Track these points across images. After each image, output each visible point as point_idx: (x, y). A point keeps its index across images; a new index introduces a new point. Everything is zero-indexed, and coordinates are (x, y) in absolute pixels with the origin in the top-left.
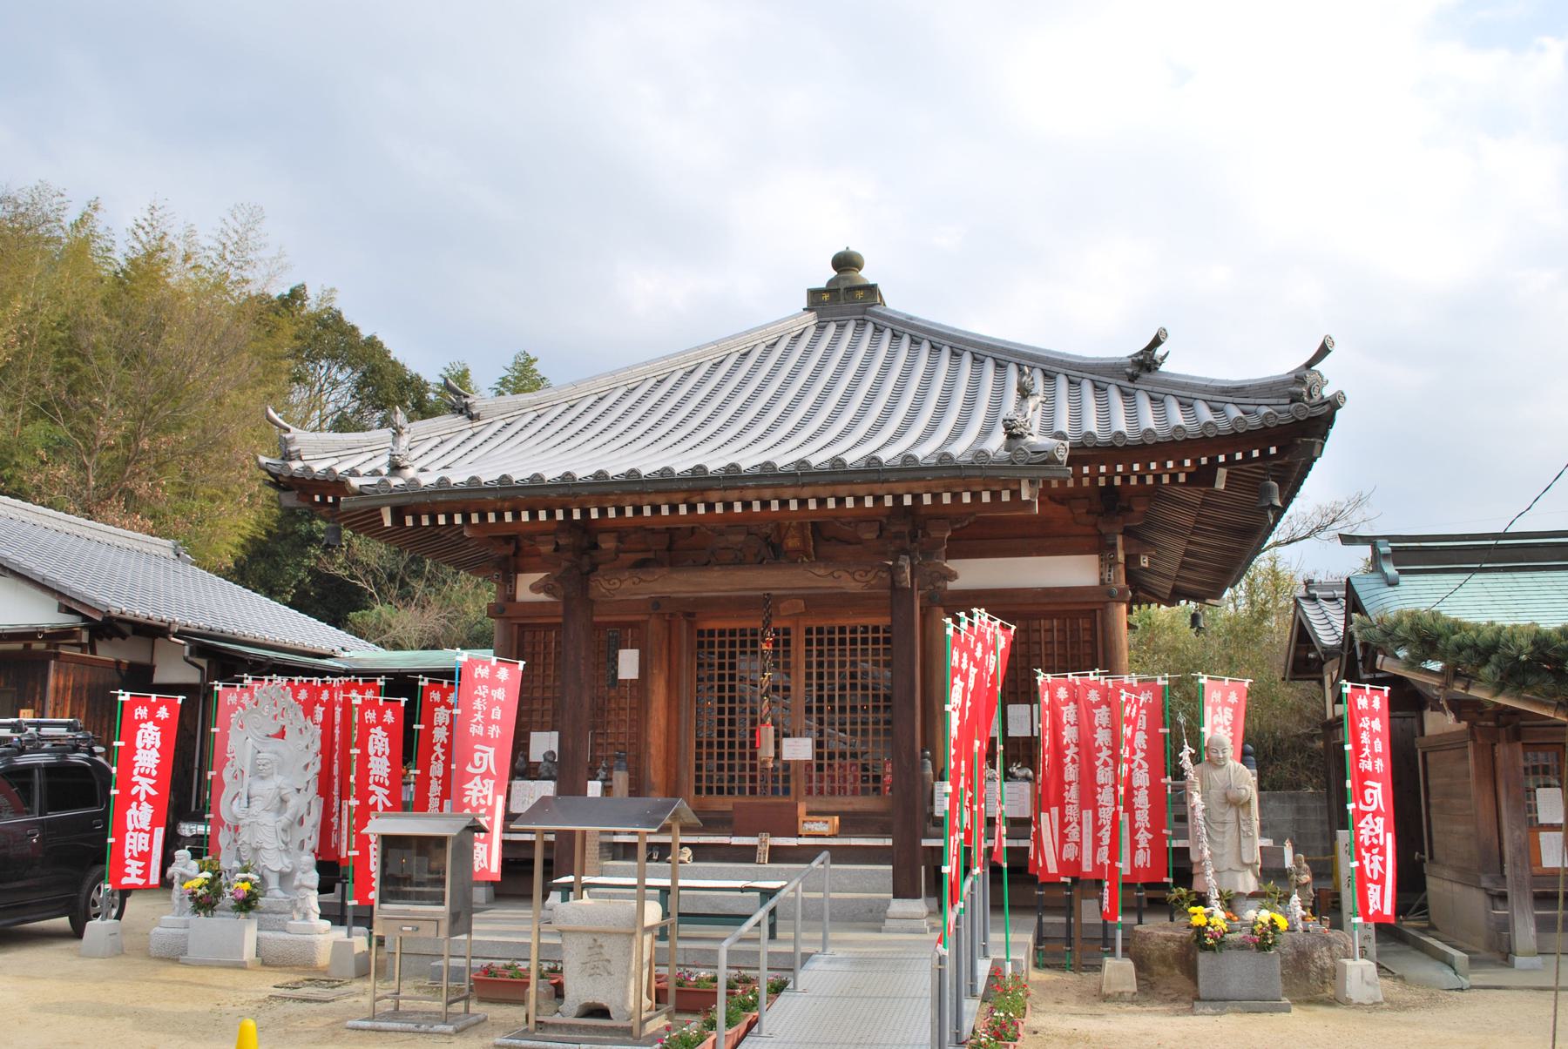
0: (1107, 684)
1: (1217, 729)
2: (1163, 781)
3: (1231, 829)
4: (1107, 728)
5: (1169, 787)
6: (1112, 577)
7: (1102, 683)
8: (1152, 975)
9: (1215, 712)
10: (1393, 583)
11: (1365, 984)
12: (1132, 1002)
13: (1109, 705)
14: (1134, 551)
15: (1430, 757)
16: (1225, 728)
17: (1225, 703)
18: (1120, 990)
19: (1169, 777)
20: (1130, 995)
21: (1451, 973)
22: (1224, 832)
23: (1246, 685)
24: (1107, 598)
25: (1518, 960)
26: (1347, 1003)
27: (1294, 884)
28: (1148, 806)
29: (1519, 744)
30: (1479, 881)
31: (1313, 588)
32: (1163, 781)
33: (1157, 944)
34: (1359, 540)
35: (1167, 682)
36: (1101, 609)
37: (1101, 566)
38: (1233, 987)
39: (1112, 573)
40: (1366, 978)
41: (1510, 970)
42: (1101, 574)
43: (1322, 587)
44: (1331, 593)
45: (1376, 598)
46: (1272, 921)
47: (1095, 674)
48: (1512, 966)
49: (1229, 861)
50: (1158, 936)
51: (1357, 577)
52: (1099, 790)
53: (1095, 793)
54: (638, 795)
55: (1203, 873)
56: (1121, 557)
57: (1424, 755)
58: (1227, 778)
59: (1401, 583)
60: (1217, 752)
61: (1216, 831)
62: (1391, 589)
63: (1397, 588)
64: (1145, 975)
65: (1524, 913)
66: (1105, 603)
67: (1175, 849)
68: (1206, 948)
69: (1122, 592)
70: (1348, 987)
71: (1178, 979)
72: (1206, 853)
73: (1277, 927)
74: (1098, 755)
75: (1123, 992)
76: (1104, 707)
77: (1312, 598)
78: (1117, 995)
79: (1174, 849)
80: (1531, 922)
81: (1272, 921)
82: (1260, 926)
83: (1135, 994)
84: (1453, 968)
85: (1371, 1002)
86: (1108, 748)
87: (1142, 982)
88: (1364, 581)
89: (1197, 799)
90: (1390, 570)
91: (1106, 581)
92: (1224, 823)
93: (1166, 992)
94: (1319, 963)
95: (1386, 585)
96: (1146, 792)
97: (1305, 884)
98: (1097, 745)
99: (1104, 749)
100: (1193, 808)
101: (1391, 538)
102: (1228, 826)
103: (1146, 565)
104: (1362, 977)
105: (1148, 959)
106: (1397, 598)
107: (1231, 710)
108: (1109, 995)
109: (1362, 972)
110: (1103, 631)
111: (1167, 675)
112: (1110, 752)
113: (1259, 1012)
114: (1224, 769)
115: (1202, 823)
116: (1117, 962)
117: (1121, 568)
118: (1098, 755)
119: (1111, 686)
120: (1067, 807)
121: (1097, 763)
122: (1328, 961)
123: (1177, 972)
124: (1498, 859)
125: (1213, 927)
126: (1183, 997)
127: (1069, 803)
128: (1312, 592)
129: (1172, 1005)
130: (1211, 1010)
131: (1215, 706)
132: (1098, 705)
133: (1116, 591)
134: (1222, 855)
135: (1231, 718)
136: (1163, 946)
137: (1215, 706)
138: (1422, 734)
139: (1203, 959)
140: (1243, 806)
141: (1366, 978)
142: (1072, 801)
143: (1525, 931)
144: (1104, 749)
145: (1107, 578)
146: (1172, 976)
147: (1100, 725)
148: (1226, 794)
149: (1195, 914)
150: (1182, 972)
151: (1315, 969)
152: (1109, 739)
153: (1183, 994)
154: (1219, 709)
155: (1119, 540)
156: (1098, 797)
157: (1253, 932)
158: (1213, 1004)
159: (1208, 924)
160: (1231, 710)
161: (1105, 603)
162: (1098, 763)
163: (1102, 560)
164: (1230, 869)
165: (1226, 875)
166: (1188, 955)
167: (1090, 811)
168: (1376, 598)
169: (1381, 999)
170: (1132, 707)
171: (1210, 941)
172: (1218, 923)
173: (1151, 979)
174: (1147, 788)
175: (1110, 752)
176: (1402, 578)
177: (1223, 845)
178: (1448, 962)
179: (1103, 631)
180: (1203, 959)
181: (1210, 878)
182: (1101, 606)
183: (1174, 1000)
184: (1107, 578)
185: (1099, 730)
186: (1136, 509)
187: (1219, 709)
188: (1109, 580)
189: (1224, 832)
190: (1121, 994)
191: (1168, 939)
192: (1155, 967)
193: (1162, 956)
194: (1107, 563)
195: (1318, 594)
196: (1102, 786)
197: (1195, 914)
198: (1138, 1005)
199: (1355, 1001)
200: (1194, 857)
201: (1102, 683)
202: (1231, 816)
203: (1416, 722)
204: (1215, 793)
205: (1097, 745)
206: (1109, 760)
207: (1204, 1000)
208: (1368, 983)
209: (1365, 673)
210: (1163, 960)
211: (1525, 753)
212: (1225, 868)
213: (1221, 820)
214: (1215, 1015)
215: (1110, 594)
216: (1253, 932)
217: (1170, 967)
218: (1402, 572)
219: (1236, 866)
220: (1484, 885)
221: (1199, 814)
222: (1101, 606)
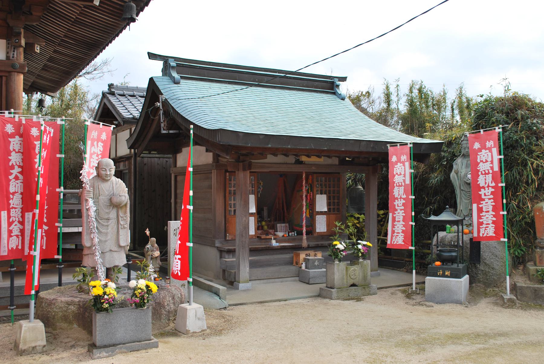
0: (20, 120)
1: (93, 156)
2: (58, 190)
3: (112, 223)
4: (19, 152)
5: (62, 194)
6: (15, 56)
7: (17, 119)
8: (55, 329)
9: (92, 145)
10: (176, 83)
11: (197, 320)
12: (43, 352)
13: (21, 136)
14: (31, 41)
15: (179, 178)
16: (98, 156)
17: (99, 140)
18: (33, 345)
19: (62, 188)
20: (41, 347)
21: (217, 298)
22: (108, 226)
23: (112, 129)
24: (11, 69)
25: (241, 286)
26: (186, 333)
27: (149, 258)
28: (21, 206)
29: (248, 172)
30: (214, 244)
31: (113, 88)
32: (58, 190)
33: (60, 308)
34: (158, 57)
35: (63, 123)
36: (6, 76)
37: (8, 48)
38: (120, 334)
39: (15, 53)
40: (198, 316)
41: (237, 291)
42: (8, 53)
43: (118, 88)
44: (122, 92)
45: (169, 89)
46: (147, 286)
47: (10, 113)
48: (238, 289)
49: (111, 244)
50: (62, 301)
51: (157, 77)
52: (11, 196)
53: (9, 199)
54: (469, 156)
55: (93, 254)
56: (23, 42)
57: (176, 177)
58: (111, 189)
59: (181, 83)
60: (106, 170)
61: (103, 225)
62: (176, 85)
63: (179, 85)
64: (50, 329)
65: (244, 260)
66: (10, 72)
67: (64, 234)
68: (101, 310)
69: (22, 66)
70: (187, 323)
71: (76, 331)
72: (96, 240)
73: (151, 291)
74: (12, 171)
75: (36, 347)
76: (17, 137)
77: (113, 94)
78: (31, 349)
79: (63, 233)
80: (247, 264)
81: (147, 286)
82: (140, 291)
83: (44, 346)
84: (219, 296)
85: (200, 330)
86: (19, 166)
87: (49, 335)
88: (161, 80)
89: (91, 202)
90: (175, 75)
91: (11, 58)
92: (108, 219)
93: (66, 340)
94: (167, 308)
95: (173, 83)
96: (20, 196)
97: (157, 257)
98: (10, 164)
99: (16, 167)
100: (88, 210)
101: (176, 59)
102: (110, 221)
103: (38, 51)
104: (196, 316)
105: (54, 318)
106: (180, 90)
107: (102, 144)
108: (24, 350)
109: (196, 312)
110: (7, 91)
111: (64, 118)
112: (20, 170)
113: (138, 350)
114: (109, 182)
115: (94, 220)
116: (31, 325)
117: (21, 50)
118: (12, 171)
119: (24, 122)
120: (12, 210)
121: (11, 177)
122: (172, 306)
123: (75, 326)
124: (224, 231)
125: (108, 295)
126: (78, 343)
127: (13, 208)
128: (113, 90)
129: (72, 351)
130: (105, 354)
131: (93, 141)
132: (12, 136)
133: (18, 66)
134: (106, 241)
135: (102, 150)
136: (65, 309)
137: (93, 141)
138: (176, 166)
139: (99, 319)
140: (121, 208)
141: (198, 316)
142: (15, 206)
143: (245, 271)
144: (16, 167)
145: (11, 56)
146: (71, 329)
147: (14, 150)
148: (110, 200)
149: (95, 287)
150: (79, 326)
151: (165, 312)
152: (20, 161)
153: (79, 341)
154: (95, 143)
155: (22, 31)
156: (11, 201)
157: (134, 295)
158: (106, 349)
159: (105, 293)
160: (102, 144)
161: (10, 72)
162: (11, 177)
163: (9, 44)
164: (111, 250)
165: (108, 255)
166: (84, 314)
167: (6, 212)
168: (169, 89)
169: (205, 328)
170: (47, 137)
171: (106, 306)
172: (112, 292)
173: (54, 332)
174: (22, 194)
175: (20, 170)
176: (182, 81)
177: (106, 234)
178: (216, 293)
179: (7, 91)
180: (99, 319)
181: (98, 258)
182: (7, 74)
183: (73, 346)
184: (11, 56)
185: (13, 154)
186: (34, 13)
187: (95, 143)
188: (13, 57)
189: (108, 226)
190: (34, 348)
191: (68, 304)
192: (58, 324)
193: (64, 316)
194: (12, 46)
195: (116, 92)
196: (13, 194)
197: (95, 287)
198: (47, 355)
199: (191, 331)
200: (86, 243)
201: (17, 119)
202: (113, 214)
203: (171, 160)
204: (103, 199)
205: (10, 164)
206: (19, 175)
207: (100, 347)
208: (199, 319)
209: (164, 130)
210: (65, 318)
211: (250, 176)
212: (108, 250)
213: (106, 217)
214: (108, 357)
215: (13, 66)
216: (134, 295)
217: (70, 323)
218: (182, 77)
219: (115, 248)
220: (217, 245)
221: (92, 213)
222: (7, 74)
